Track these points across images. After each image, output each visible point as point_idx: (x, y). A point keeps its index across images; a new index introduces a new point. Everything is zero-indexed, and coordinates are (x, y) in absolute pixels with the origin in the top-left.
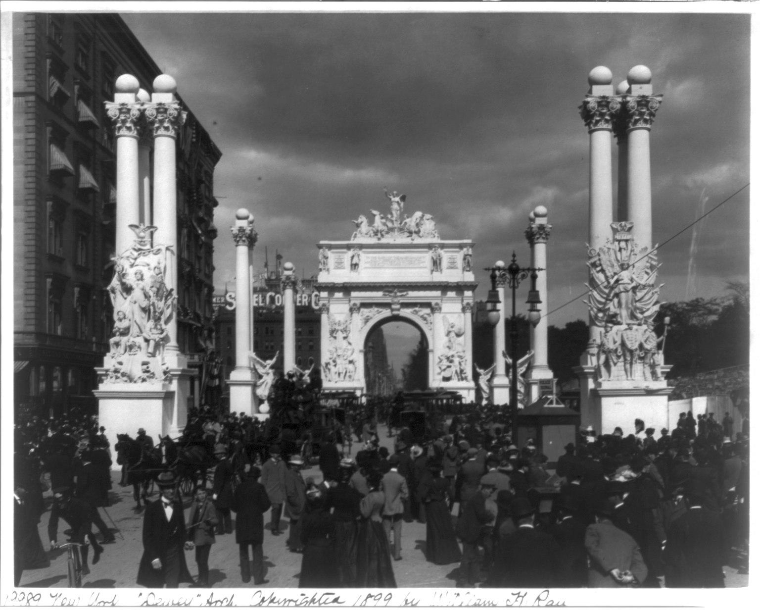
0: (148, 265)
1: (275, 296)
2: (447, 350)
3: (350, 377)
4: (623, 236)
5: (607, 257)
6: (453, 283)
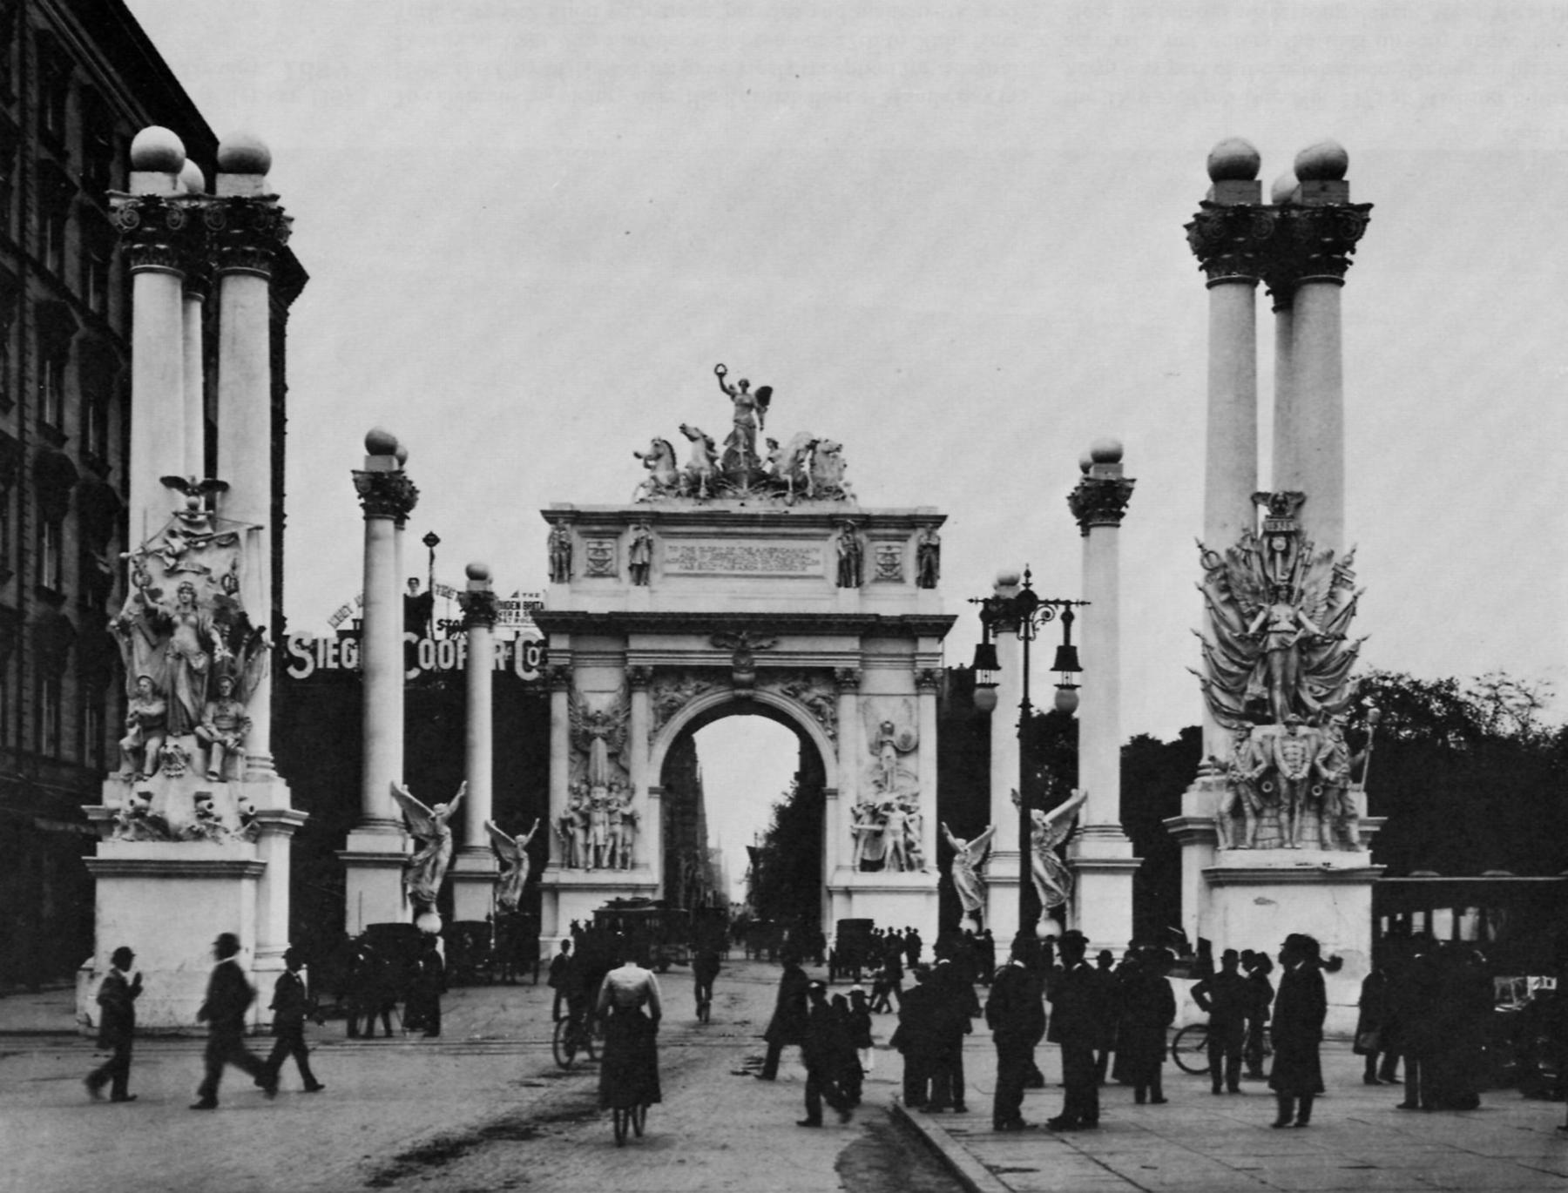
0: (207, 570)
1: (419, 641)
2: (873, 788)
3: (624, 858)
4: (1279, 524)
5: (1243, 569)
6: (892, 618)
